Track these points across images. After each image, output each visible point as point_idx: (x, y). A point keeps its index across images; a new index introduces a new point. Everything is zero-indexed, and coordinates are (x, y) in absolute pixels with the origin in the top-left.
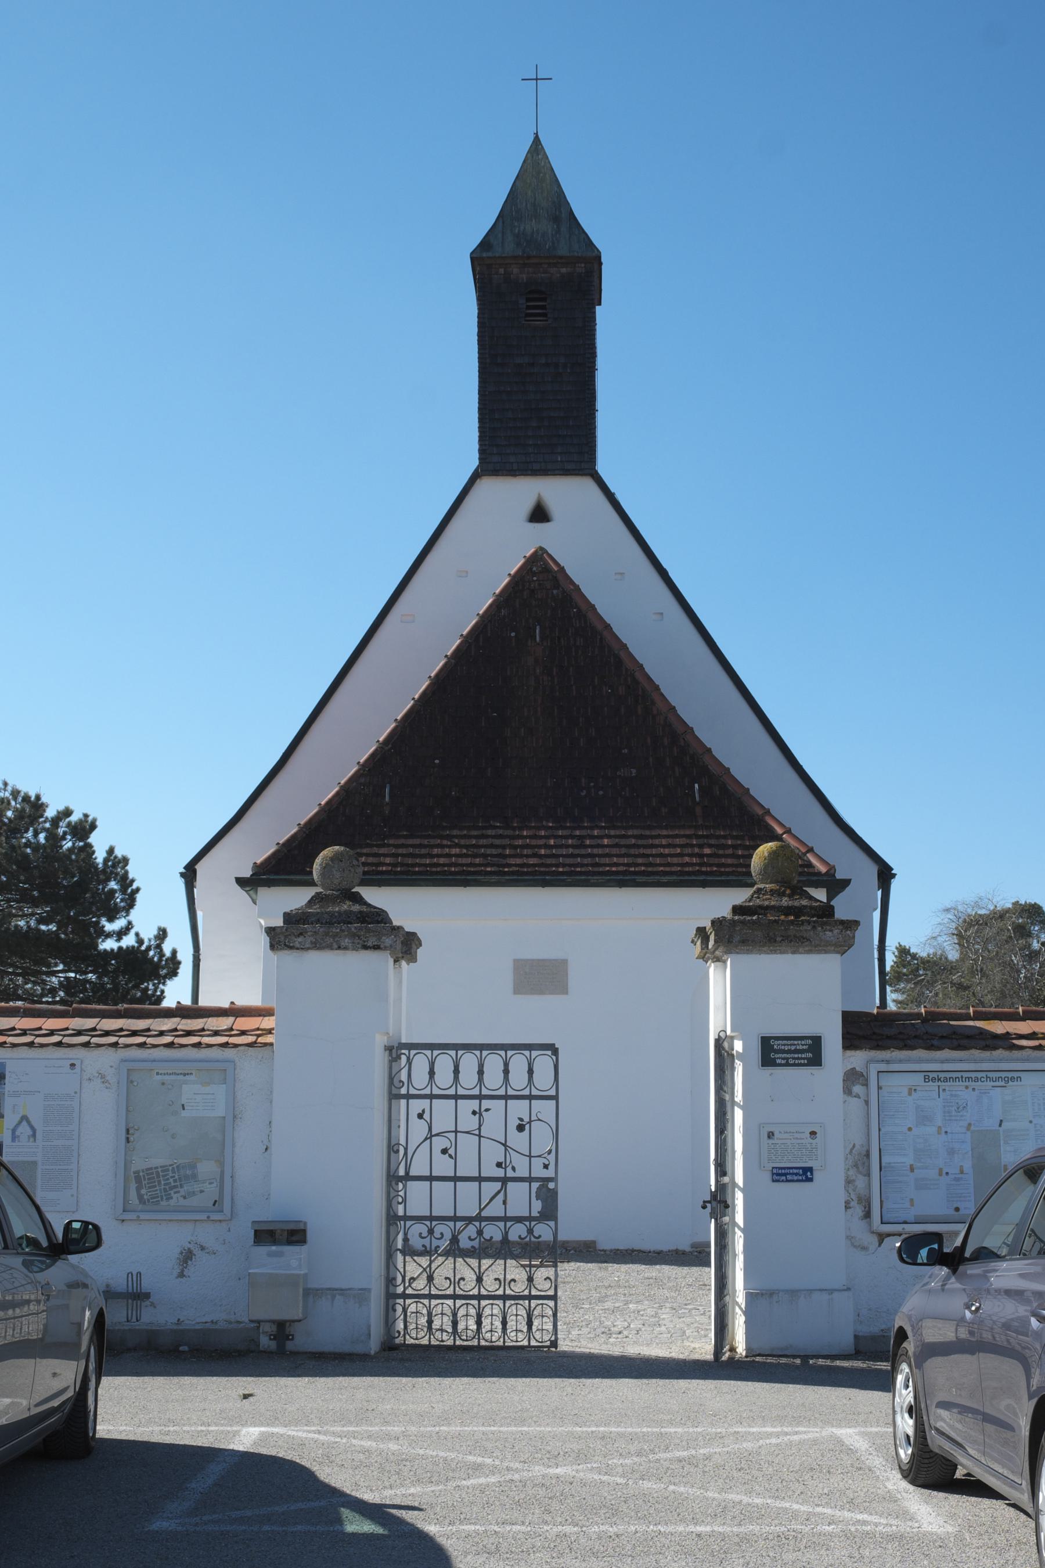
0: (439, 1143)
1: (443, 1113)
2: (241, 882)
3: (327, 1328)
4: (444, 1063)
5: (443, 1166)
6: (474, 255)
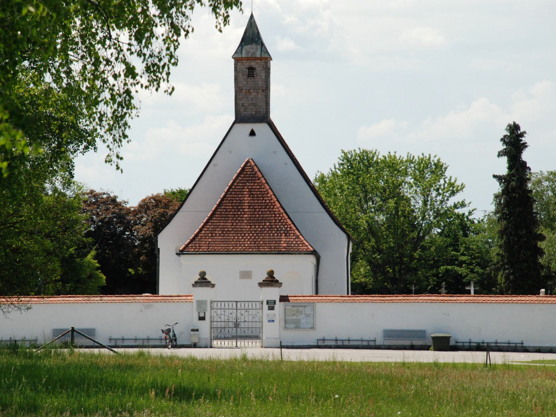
0: (218, 316)
1: (219, 311)
2: (177, 254)
3: (202, 343)
4: (219, 304)
5: (219, 320)
6: (236, 56)
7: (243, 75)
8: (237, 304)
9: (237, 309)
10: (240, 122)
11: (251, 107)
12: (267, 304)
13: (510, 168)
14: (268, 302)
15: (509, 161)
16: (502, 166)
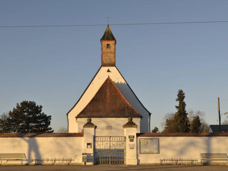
0: (99, 146)
7: (105, 47)
8: (110, 138)
9: (110, 141)
10: (103, 66)
11: (108, 60)
12: (129, 138)
13: (180, 104)
14: (129, 137)
15: (180, 102)
16: (177, 104)
